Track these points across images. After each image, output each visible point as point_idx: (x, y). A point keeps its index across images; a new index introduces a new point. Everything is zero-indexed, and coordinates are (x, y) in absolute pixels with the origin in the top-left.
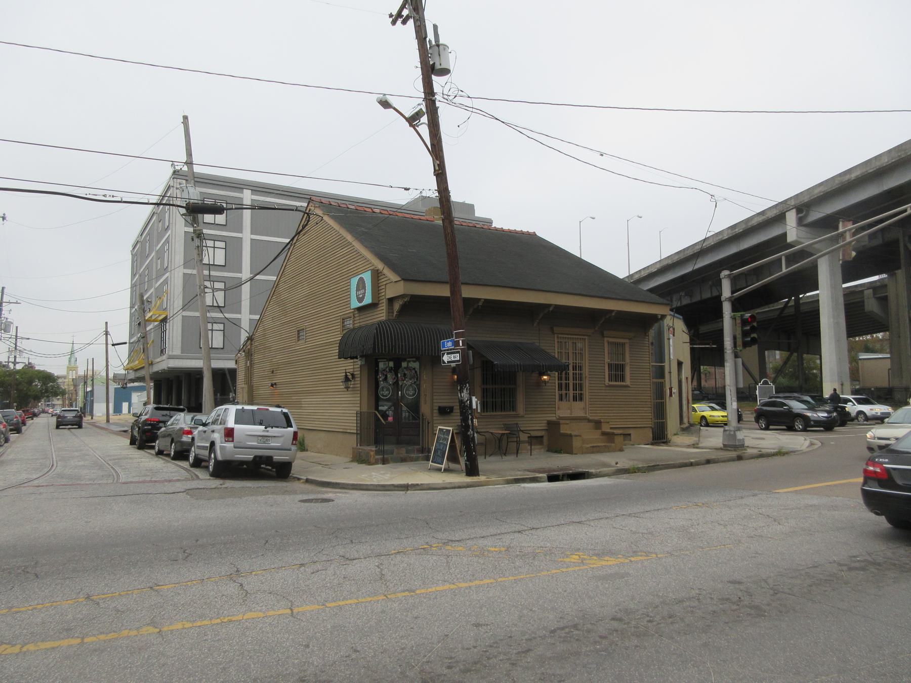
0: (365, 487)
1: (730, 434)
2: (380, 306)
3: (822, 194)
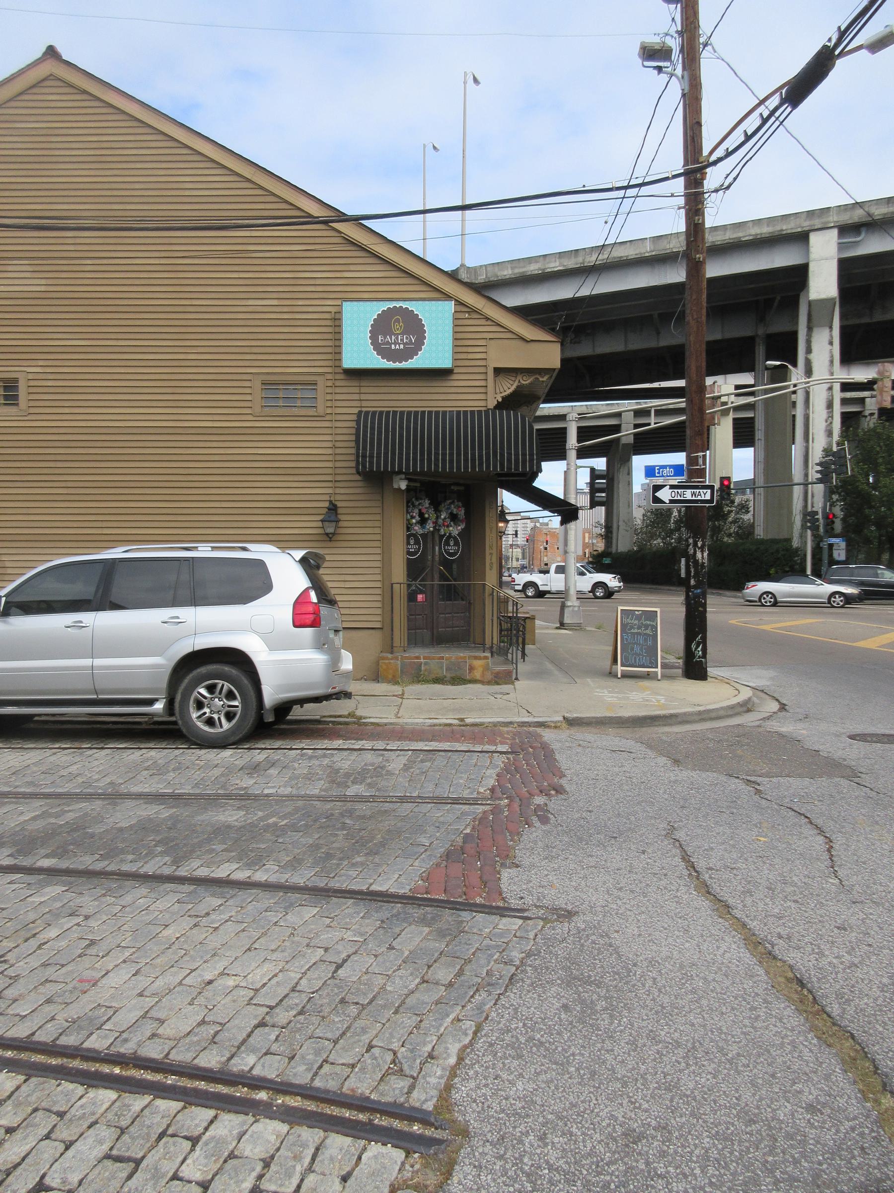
0: (713, 715)
1: (573, 611)
2: (455, 377)
3: (751, 238)
